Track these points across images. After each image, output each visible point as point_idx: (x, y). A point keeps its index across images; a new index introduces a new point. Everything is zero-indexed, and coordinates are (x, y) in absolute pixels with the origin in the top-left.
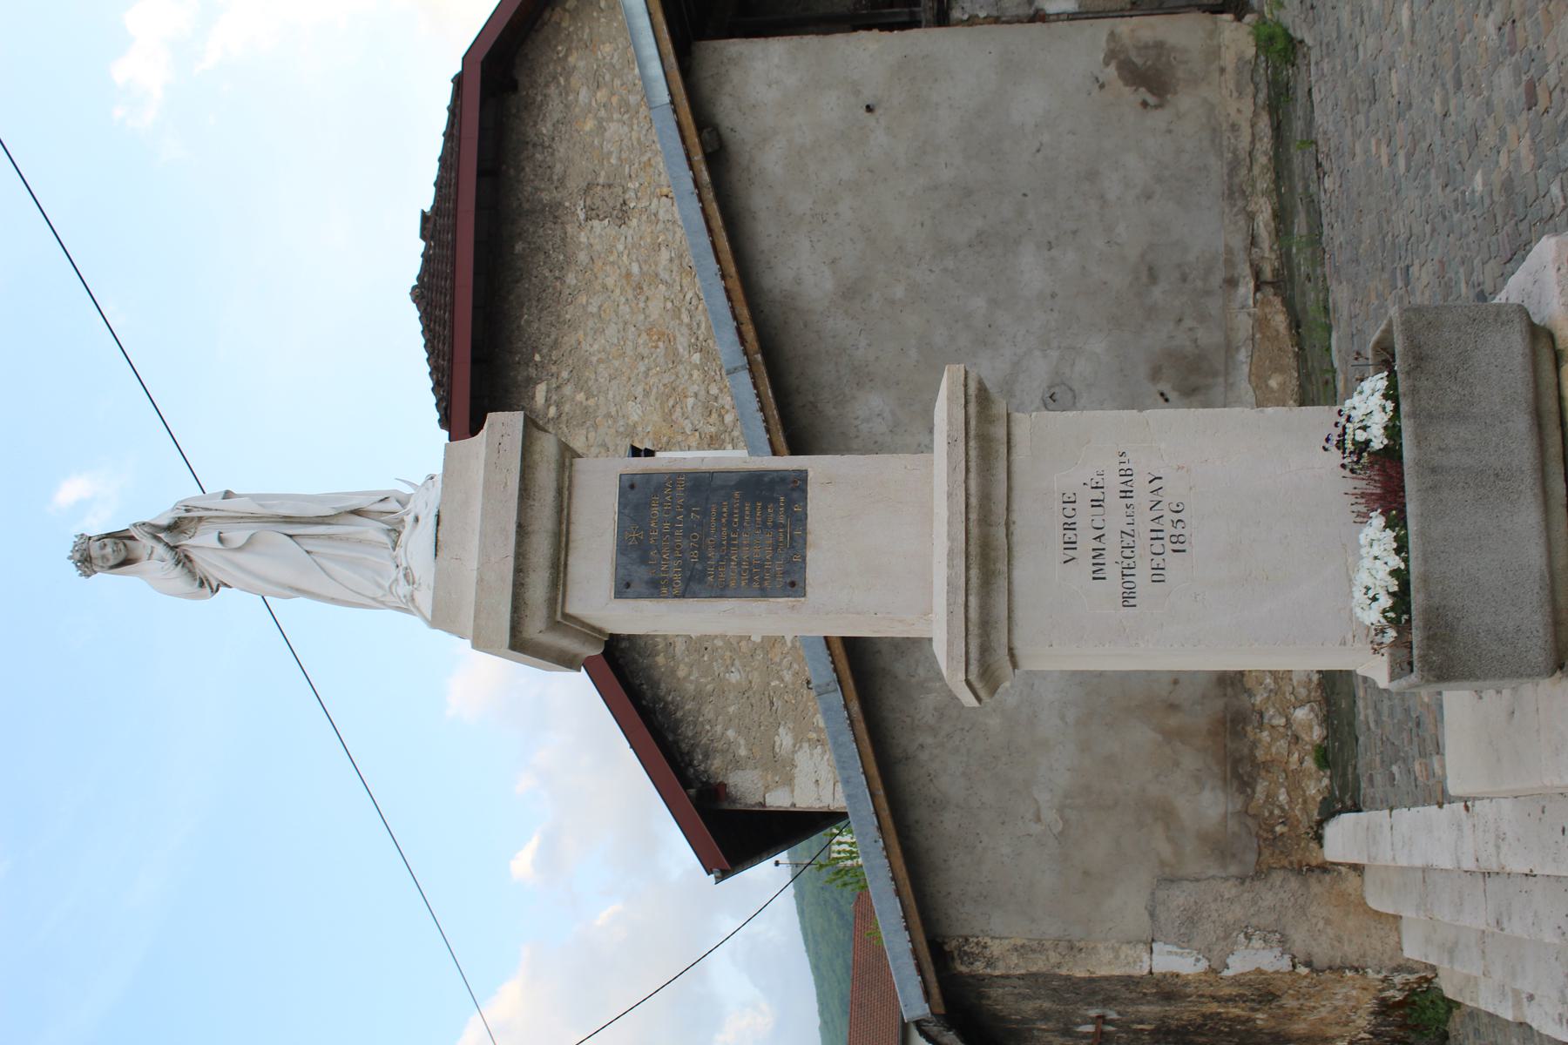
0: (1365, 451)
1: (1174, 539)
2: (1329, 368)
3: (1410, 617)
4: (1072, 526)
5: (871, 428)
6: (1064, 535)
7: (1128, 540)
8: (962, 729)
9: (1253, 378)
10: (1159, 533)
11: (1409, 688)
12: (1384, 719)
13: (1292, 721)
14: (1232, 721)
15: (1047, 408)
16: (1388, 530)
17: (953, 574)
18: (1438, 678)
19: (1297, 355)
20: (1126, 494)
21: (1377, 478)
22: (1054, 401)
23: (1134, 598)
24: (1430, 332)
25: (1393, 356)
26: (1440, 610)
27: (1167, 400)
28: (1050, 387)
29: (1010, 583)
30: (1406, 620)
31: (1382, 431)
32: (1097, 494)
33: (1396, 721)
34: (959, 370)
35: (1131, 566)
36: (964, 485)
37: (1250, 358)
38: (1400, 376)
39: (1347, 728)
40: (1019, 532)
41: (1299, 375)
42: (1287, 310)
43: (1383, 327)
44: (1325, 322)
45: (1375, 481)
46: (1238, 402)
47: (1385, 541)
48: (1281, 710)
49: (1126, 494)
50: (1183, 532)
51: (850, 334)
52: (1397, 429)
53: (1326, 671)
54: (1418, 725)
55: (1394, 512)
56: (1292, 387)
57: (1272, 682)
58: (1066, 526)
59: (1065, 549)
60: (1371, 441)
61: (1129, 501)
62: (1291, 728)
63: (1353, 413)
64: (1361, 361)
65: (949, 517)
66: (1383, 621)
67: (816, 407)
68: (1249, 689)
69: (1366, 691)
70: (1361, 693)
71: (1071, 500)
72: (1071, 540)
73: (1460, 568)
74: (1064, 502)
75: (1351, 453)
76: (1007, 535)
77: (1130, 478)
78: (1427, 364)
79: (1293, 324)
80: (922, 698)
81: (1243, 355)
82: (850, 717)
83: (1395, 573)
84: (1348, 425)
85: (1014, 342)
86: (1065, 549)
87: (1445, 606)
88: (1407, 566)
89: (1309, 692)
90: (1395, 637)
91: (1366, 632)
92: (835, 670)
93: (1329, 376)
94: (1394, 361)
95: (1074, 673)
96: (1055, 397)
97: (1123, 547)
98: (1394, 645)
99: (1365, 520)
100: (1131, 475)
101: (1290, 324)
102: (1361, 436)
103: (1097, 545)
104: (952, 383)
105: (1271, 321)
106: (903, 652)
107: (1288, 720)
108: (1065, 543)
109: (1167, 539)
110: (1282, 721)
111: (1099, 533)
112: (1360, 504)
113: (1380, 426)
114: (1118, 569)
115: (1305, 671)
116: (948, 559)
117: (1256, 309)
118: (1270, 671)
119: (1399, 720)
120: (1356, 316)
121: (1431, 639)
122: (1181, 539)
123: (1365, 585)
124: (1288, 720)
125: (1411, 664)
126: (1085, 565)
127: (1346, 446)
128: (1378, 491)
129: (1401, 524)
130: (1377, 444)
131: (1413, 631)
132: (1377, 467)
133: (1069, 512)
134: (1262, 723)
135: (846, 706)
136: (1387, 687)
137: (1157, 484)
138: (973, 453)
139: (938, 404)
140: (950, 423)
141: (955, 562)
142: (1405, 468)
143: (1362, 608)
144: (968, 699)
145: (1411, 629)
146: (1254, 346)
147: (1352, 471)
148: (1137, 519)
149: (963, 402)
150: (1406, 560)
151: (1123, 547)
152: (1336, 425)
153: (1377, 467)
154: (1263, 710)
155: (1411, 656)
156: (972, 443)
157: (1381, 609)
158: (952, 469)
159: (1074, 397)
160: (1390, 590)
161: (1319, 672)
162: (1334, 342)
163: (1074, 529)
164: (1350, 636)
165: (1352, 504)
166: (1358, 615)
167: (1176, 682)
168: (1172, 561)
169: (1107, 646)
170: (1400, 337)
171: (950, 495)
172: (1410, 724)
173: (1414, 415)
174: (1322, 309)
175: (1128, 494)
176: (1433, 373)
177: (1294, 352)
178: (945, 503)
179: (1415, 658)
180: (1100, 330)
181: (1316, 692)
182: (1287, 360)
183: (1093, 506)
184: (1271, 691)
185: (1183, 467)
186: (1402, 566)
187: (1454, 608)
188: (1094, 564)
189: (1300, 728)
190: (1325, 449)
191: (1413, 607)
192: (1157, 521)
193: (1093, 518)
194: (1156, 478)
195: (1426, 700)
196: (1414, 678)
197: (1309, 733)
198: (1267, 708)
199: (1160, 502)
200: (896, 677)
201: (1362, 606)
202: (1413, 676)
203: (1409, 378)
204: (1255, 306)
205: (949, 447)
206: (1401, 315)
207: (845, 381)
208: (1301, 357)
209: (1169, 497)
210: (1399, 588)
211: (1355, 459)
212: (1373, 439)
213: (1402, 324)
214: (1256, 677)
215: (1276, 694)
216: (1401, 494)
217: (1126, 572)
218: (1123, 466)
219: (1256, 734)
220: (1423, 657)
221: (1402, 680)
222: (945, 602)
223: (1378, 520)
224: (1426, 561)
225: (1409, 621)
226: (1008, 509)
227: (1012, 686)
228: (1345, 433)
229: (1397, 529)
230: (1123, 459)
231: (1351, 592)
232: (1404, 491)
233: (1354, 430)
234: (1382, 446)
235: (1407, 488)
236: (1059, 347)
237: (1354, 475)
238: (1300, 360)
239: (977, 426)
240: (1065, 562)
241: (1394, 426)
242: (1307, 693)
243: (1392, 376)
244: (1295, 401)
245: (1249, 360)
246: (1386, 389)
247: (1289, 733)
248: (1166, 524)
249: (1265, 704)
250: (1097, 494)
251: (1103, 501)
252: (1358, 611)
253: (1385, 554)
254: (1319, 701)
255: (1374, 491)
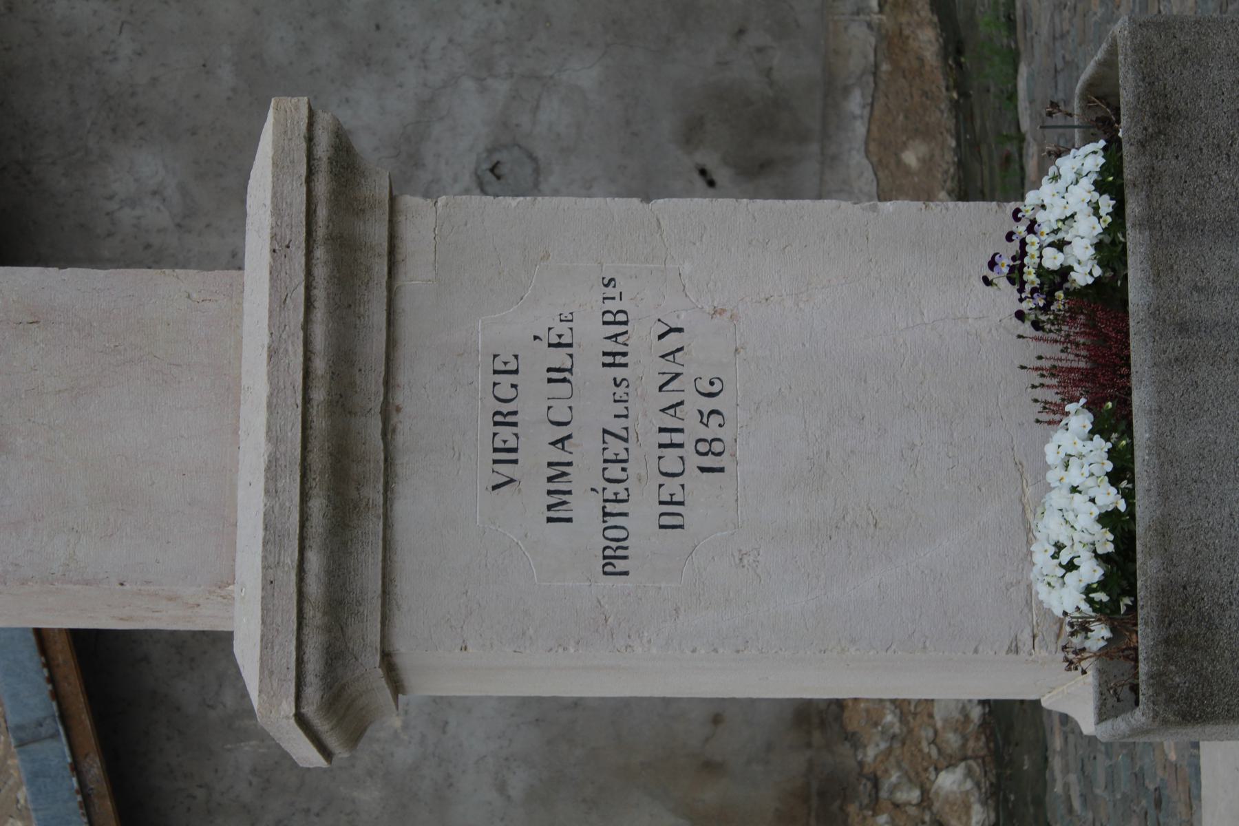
0: (1060, 288)
1: (703, 447)
2: (1013, 132)
3: (1135, 602)
4: (510, 419)
5: (139, 218)
6: (495, 434)
7: (616, 447)
8: (308, 811)
9: (873, 147)
10: (674, 435)
11: (1129, 736)
12: (1098, 791)
13: (931, 795)
14: (822, 794)
15: (484, 192)
16: (1097, 437)
17: (277, 509)
18: (1184, 718)
19: (955, 106)
20: (614, 359)
21: (1081, 340)
22: (498, 177)
23: (625, 558)
24: (1184, 67)
25: (1117, 111)
26: (1190, 590)
27: (711, 183)
28: (491, 151)
29: (387, 525)
30: (1127, 605)
31: (1092, 251)
32: (559, 358)
33: (1119, 796)
34: (297, 108)
35: (619, 497)
36: (301, 334)
37: (868, 109)
38: (1127, 149)
39: (1032, 810)
40: (407, 428)
41: (959, 144)
42: (940, 21)
43: (1099, 55)
44: (1009, 46)
45: (1077, 345)
46: (844, 191)
47: (1091, 458)
48: (912, 774)
49: (614, 359)
50: (720, 433)
51: (100, 29)
52: (1120, 248)
53: (996, 701)
54: (1158, 804)
55: (1110, 404)
56: (945, 166)
57: (896, 720)
58: (499, 418)
59: (495, 462)
60: (1071, 268)
61: (619, 373)
62: (930, 807)
63: (1041, 216)
64: (1059, 119)
65: (270, 396)
66: (1085, 607)
67: (29, 173)
68: (854, 734)
69: (1066, 739)
70: (1057, 743)
71: (509, 368)
72: (508, 446)
73: (1227, 510)
74: (495, 372)
75: (1034, 291)
76: (384, 434)
77: (622, 328)
78: (1177, 128)
79: (951, 48)
80: (229, 750)
81: (855, 103)
82: (83, 789)
83: (1108, 519)
84: (1030, 238)
85: (423, 61)
86: (495, 462)
87: (1197, 583)
88: (1131, 505)
89: (965, 739)
90: (1108, 640)
91: (1056, 628)
92: (56, 695)
93: (1011, 148)
94: (1118, 122)
95: (525, 702)
96: (500, 171)
97: (606, 461)
98: (1105, 653)
99: (1057, 417)
100: (625, 323)
101: (945, 48)
102: (1053, 260)
103: (557, 455)
104: (282, 133)
105: (911, 41)
106: (192, 660)
107: (925, 792)
108: (496, 450)
109: (690, 447)
110: (915, 795)
111: (562, 432)
112: (1048, 386)
113: (1087, 242)
114: (596, 502)
115: (958, 701)
116: (267, 480)
117: (884, 17)
118: (893, 701)
119: (1125, 796)
120: (1063, 36)
121: (1170, 642)
122: (717, 447)
123: (1054, 538)
124: (925, 792)
125: (1135, 689)
126: (535, 494)
127: (1025, 278)
128: (1082, 365)
129: (1122, 427)
130: (1081, 277)
131: (1140, 628)
132: (1082, 318)
133: (505, 391)
134: (877, 798)
135: (76, 768)
136: (1094, 734)
137: (673, 341)
138: (320, 272)
139: (254, 174)
140: (277, 211)
141: (280, 485)
142: (1132, 323)
143: (1049, 584)
144: (305, 753)
145: (1136, 625)
146: (876, 83)
147: (1037, 325)
148: (635, 406)
149: (303, 170)
150: (1129, 496)
151: (606, 461)
152: (1009, 237)
153: (1082, 318)
154: (879, 773)
155: (1136, 675)
156: (320, 253)
157: (1083, 584)
158: (278, 303)
159: (537, 171)
160: (1100, 551)
161: (983, 703)
162: (1022, 84)
163: (515, 424)
164: (1026, 636)
165: (1034, 387)
166: (1041, 597)
167: (717, 720)
168: (698, 487)
169: (572, 650)
170: (1130, 76)
171: (273, 353)
172: (1144, 803)
173: (1149, 223)
174: (1003, 19)
175: (619, 359)
176: (1187, 146)
177: (951, 100)
178: (263, 368)
179: (1142, 677)
180: (589, 45)
181: (978, 739)
182: (938, 114)
183: (550, 381)
184: (894, 737)
185: (723, 311)
186: (1122, 506)
187: (1215, 585)
188: (550, 493)
189: (947, 809)
190: (987, 282)
191: (1139, 584)
192: (671, 411)
193: (551, 403)
194: (671, 330)
195: (1173, 756)
196: (1139, 717)
197: (964, 819)
198: (886, 771)
199: (677, 375)
200: (178, 709)
201: (1048, 579)
202: (1138, 712)
203: (1144, 154)
204: (881, 10)
205: (274, 259)
206: (1133, 34)
207: (88, 124)
208: (963, 110)
209: (695, 366)
210: (1116, 547)
211: (1041, 303)
212: (1076, 267)
213: (1135, 51)
214: (867, 711)
215: (903, 744)
216: (1124, 371)
217: (611, 508)
218: (609, 305)
219: (865, 818)
220: (1158, 679)
221: (1119, 719)
222: (258, 560)
223: (1079, 420)
224: (1164, 496)
225: (1132, 609)
226: (389, 383)
227: (405, 727)
228: (1023, 253)
229: (1114, 436)
230: (610, 291)
231: (1031, 553)
232: (1129, 367)
233: (1041, 248)
234: (1090, 280)
235: (1135, 358)
236: (511, 75)
237: (1040, 334)
238: (961, 117)
239: (330, 220)
240: (494, 488)
241: (1114, 242)
242: (960, 742)
243: (1113, 151)
244: (950, 193)
245: (866, 112)
246: (1100, 173)
247: (927, 818)
248: (689, 418)
249: (882, 762)
250: (559, 358)
251: (570, 371)
252: (1042, 591)
253: (1091, 482)
254: (983, 758)
255: (1074, 365)
